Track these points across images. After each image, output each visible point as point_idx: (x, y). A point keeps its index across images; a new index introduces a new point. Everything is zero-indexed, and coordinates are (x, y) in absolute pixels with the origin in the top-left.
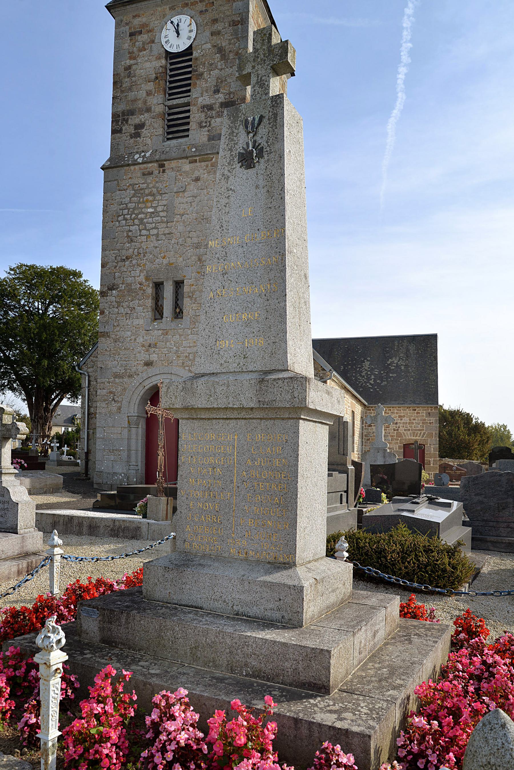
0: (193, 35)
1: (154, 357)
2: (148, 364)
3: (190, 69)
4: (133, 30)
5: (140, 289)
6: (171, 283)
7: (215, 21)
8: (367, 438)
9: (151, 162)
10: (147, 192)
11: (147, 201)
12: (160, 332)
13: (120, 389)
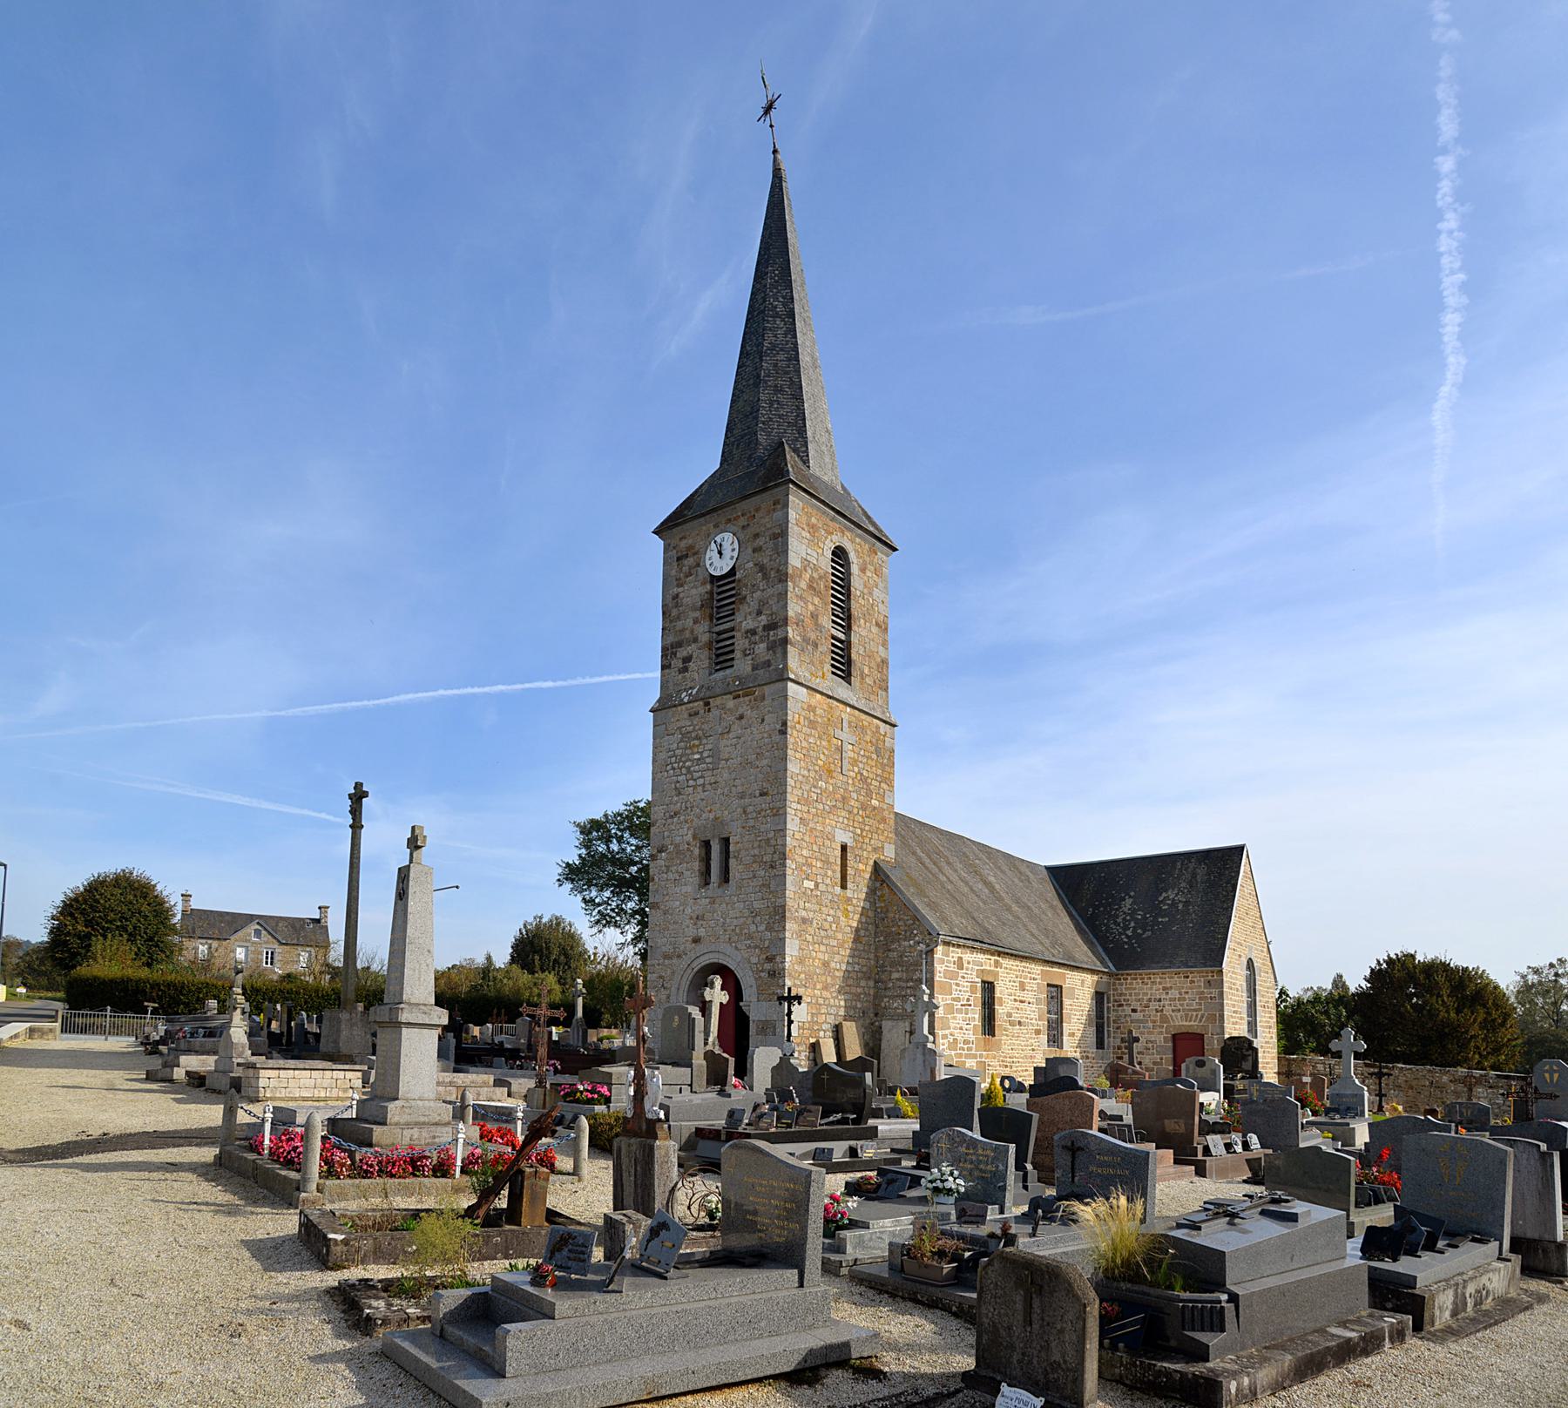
0: (735, 554)
1: (702, 932)
2: (696, 940)
3: (733, 592)
4: (679, 554)
5: (688, 849)
6: (717, 841)
7: (756, 536)
8: (1116, 1025)
9: (697, 701)
10: (693, 735)
11: (694, 745)
12: (708, 900)
13: (669, 972)
